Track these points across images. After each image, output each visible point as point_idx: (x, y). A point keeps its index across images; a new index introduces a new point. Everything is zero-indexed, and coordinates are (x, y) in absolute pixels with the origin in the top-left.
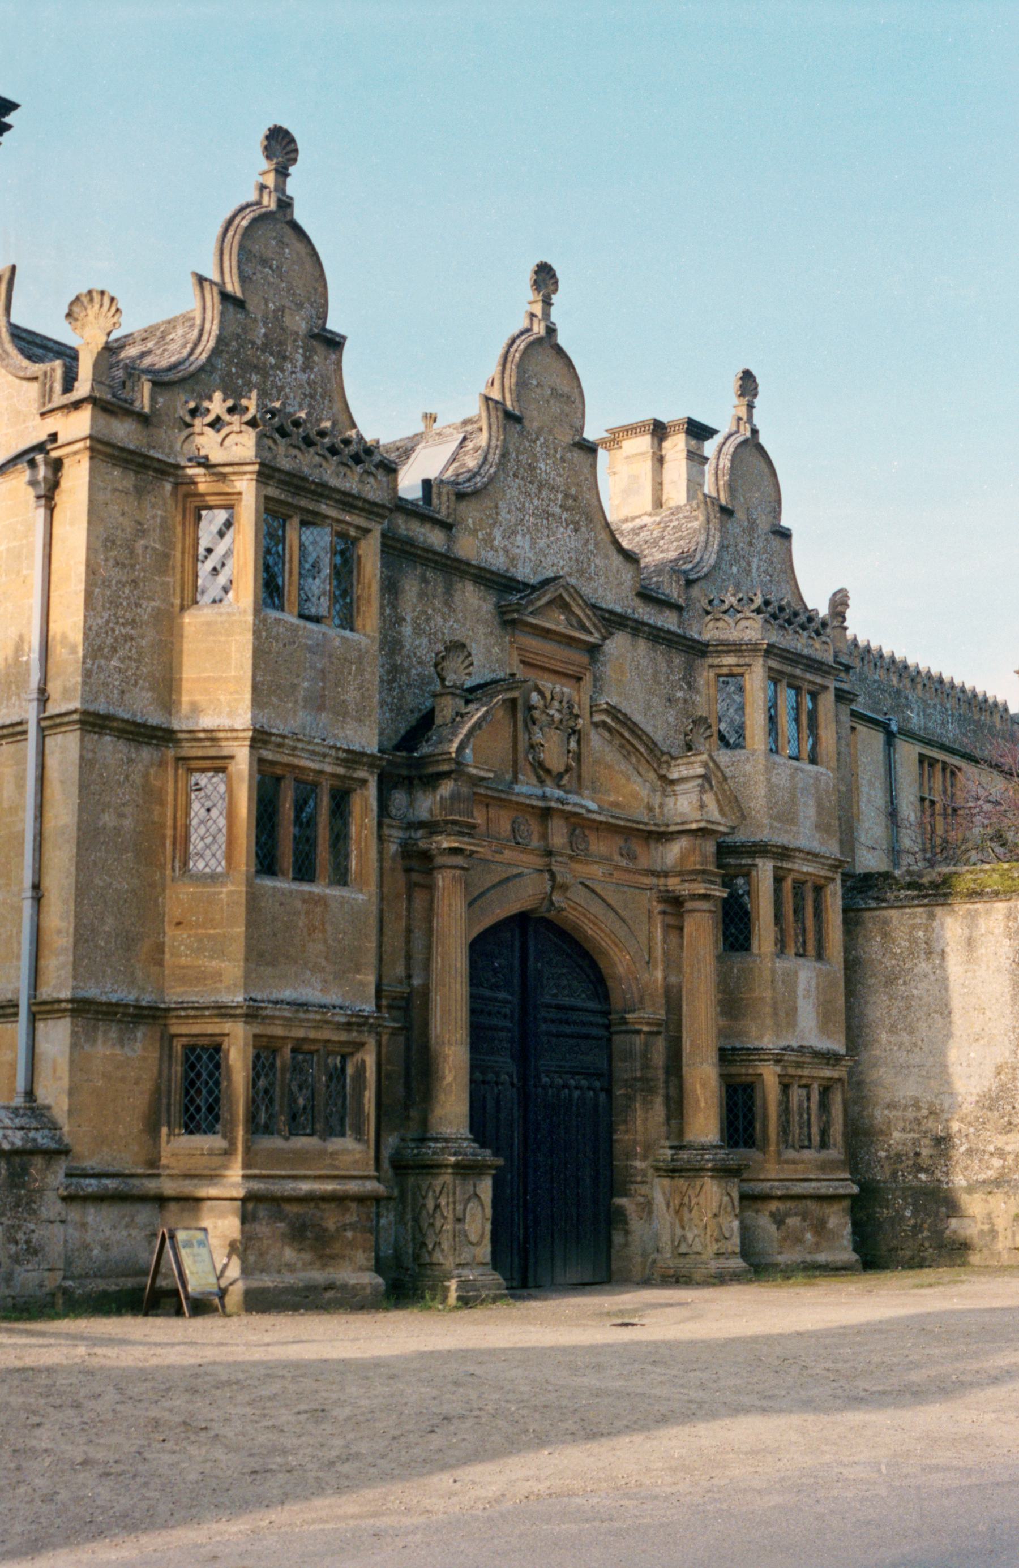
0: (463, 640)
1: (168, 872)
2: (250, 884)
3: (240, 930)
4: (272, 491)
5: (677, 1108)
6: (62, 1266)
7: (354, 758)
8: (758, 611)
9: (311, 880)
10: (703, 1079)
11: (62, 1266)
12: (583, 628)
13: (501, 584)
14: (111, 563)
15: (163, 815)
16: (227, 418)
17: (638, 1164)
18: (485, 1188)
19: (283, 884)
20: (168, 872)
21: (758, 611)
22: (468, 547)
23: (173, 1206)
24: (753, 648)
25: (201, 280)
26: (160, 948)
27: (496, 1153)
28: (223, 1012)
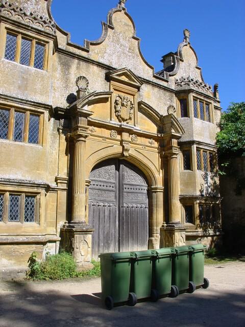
19: (26, 144)
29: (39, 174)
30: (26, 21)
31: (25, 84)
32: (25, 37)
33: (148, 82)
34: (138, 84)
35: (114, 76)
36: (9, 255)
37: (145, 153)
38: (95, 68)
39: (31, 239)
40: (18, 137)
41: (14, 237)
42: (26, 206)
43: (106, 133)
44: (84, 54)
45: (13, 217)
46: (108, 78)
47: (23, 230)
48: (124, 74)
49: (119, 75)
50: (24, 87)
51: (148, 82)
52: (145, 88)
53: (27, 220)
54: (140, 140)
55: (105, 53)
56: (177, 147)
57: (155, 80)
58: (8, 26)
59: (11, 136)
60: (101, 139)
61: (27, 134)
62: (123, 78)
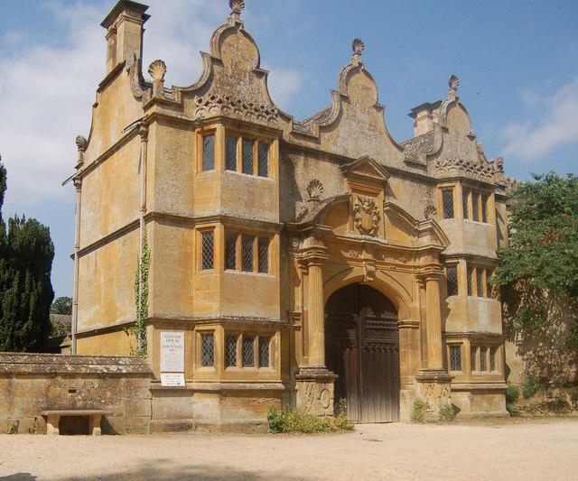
0: (450, 238)
1: (194, 270)
2: (221, 272)
3: (279, 295)
4: (229, 127)
5: (425, 355)
6: (301, 387)
7: (267, 225)
8: (457, 164)
9: (251, 271)
10: (435, 342)
11: (301, 387)
12: (378, 174)
13: (334, 158)
14: (166, 158)
15: (191, 250)
16: (210, 101)
17: (410, 377)
18: (331, 386)
20: (194, 270)
21: (457, 164)
22: (322, 148)
23: (196, 395)
24: (456, 179)
25: (203, 54)
26: (191, 298)
27: (335, 373)
28: (211, 321)
34: (383, 178)
44: (312, 145)
52: (394, 182)
57: (406, 169)
61: (255, 263)
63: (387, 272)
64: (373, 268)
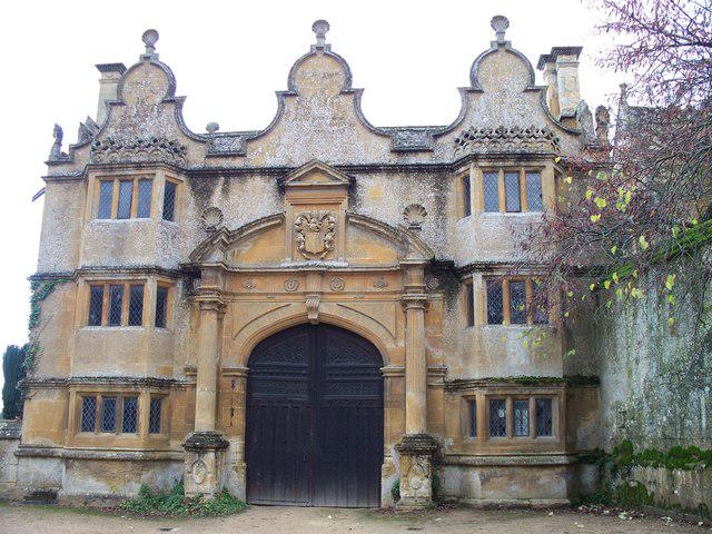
19: (123, 328)
29: (138, 367)
30: (117, 157)
31: (120, 242)
32: (124, 180)
33: (372, 169)
35: (289, 183)
36: (98, 475)
37: (360, 307)
38: (258, 181)
39: (123, 455)
40: (115, 320)
41: (505, 458)
42: (126, 412)
43: (276, 286)
44: (238, 163)
45: (108, 427)
46: (282, 189)
47: (115, 443)
48: (316, 171)
49: (299, 179)
50: (119, 250)
51: (372, 169)
52: (364, 181)
53: (127, 431)
54: (353, 285)
55: (278, 145)
56: (419, 287)
57: (394, 160)
58: (98, 174)
59: (104, 321)
60: (265, 297)
61: (125, 315)
62: (316, 180)
63: (347, 305)
64: (316, 303)
